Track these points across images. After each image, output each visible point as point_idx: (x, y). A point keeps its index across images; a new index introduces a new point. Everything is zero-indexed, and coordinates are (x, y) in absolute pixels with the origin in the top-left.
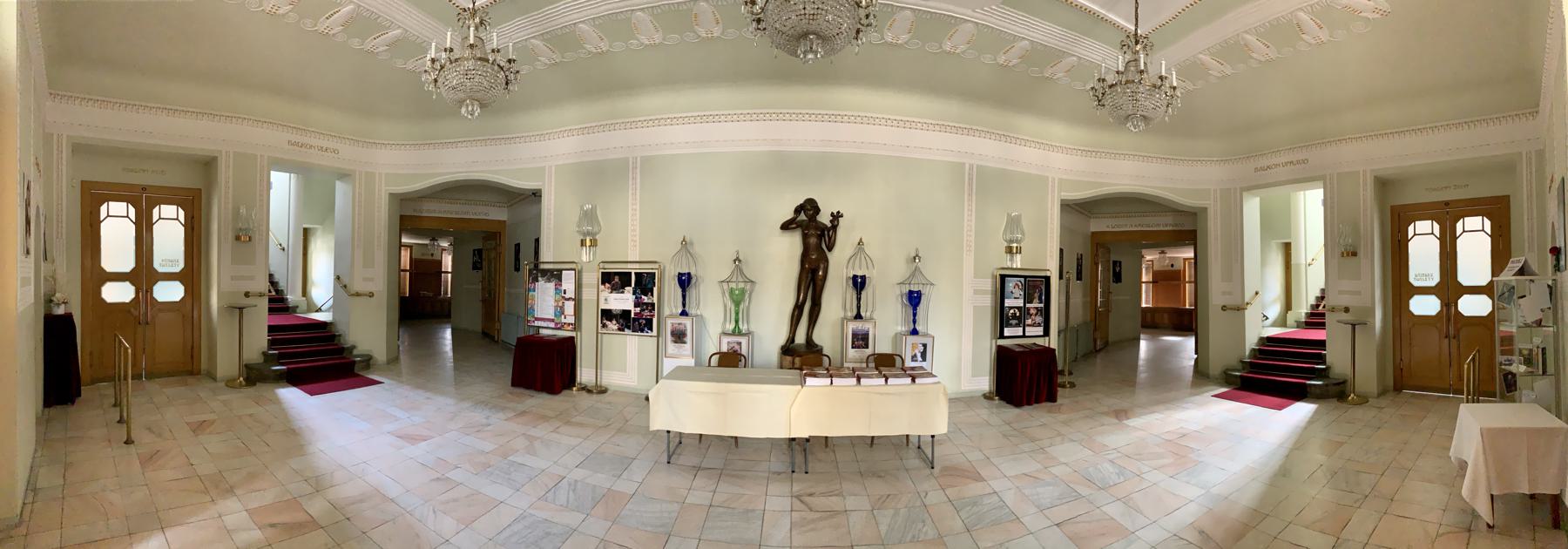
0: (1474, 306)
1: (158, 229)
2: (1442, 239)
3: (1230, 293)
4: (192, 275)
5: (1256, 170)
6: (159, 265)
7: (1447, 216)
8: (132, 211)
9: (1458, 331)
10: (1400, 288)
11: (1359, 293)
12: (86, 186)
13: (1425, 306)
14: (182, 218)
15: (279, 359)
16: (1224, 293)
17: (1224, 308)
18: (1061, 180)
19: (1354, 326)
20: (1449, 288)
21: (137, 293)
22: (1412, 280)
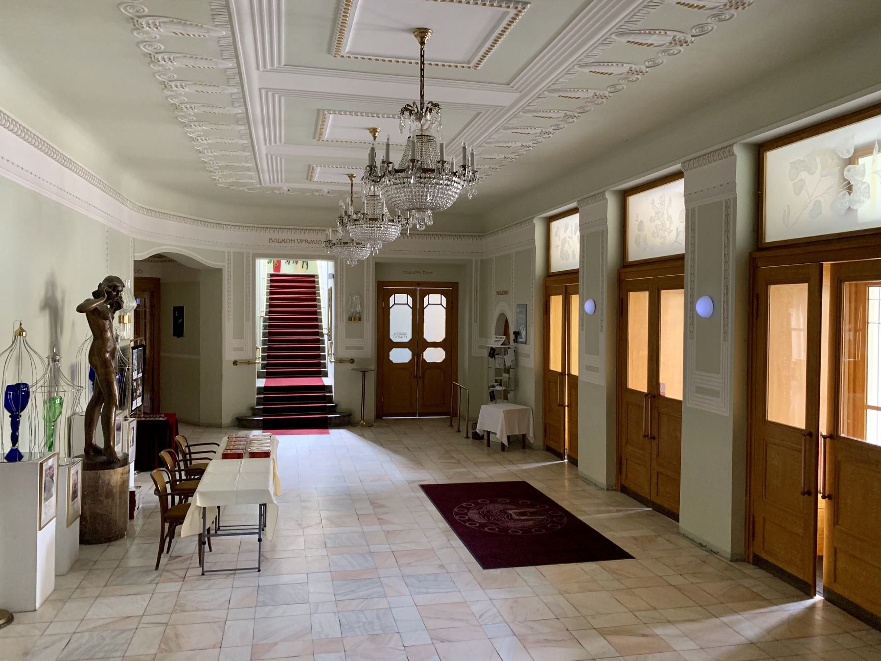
0: (434, 356)
1: (393, 312)
2: (414, 309)
3: (241, 349)
4: (450, 344)
5: (271, 240)
6: (394, 337)
7: (418, 293)
8: (410, 299)
9: (423, 373)
10: (384, 343)
11: (362, 348)
12: (455, 285)
13: (400, 356)
14: (444, 304)
15: (265, 412)
16: (235, 349)
17: (235, 363)
18: (234, 253)
19: (364, 373)
20: (418, 343)
21: (424, 360)
22: (391, 337)
